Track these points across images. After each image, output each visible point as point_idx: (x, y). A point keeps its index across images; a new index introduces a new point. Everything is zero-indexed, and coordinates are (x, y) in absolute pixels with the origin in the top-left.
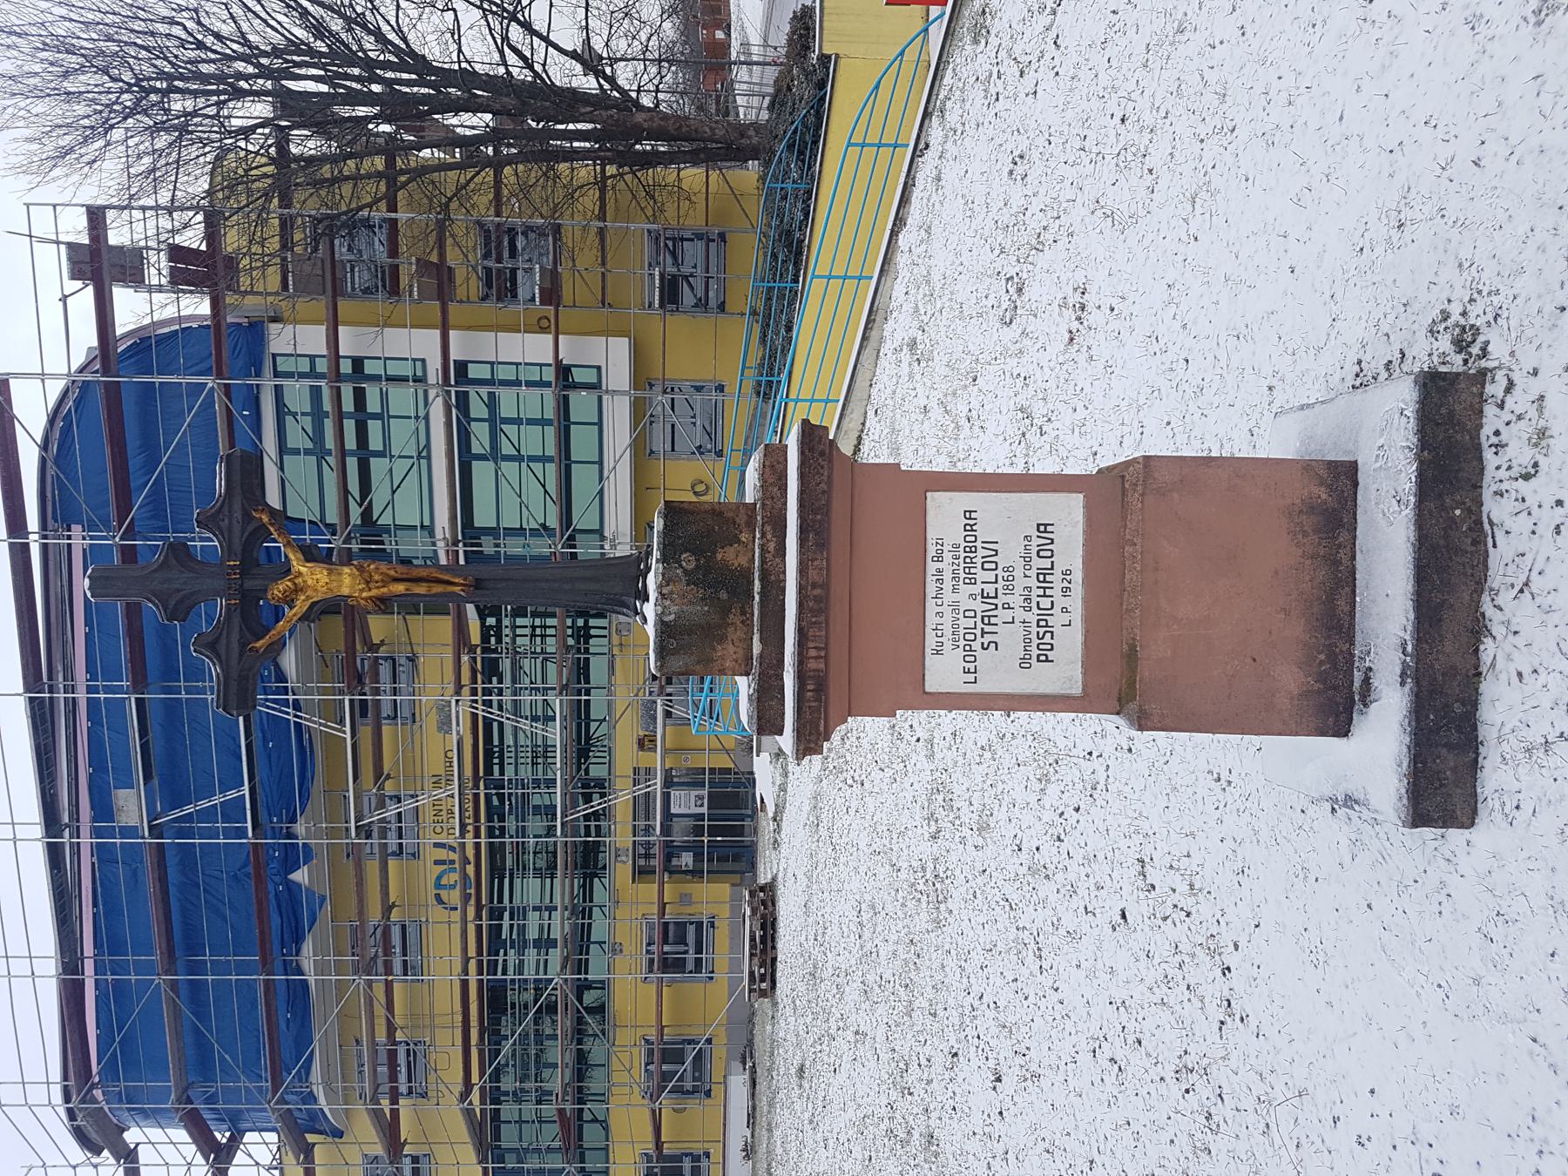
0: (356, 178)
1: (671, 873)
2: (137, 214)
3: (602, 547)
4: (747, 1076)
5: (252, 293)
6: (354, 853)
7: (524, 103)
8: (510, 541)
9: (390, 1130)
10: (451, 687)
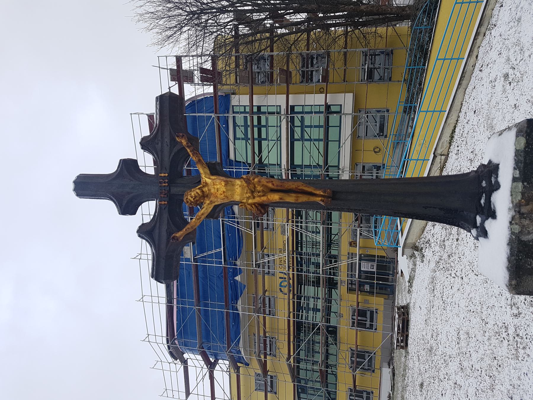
0: (261, 39)
1: (361, 291)
2: (191, 58)
3: (338, 172)
4: (390, 370)
5: (227, 85)
6: (254, 272)
7: (319, 6)
8: (306, 169)
9: (264, 366)
10: (285, 220)
